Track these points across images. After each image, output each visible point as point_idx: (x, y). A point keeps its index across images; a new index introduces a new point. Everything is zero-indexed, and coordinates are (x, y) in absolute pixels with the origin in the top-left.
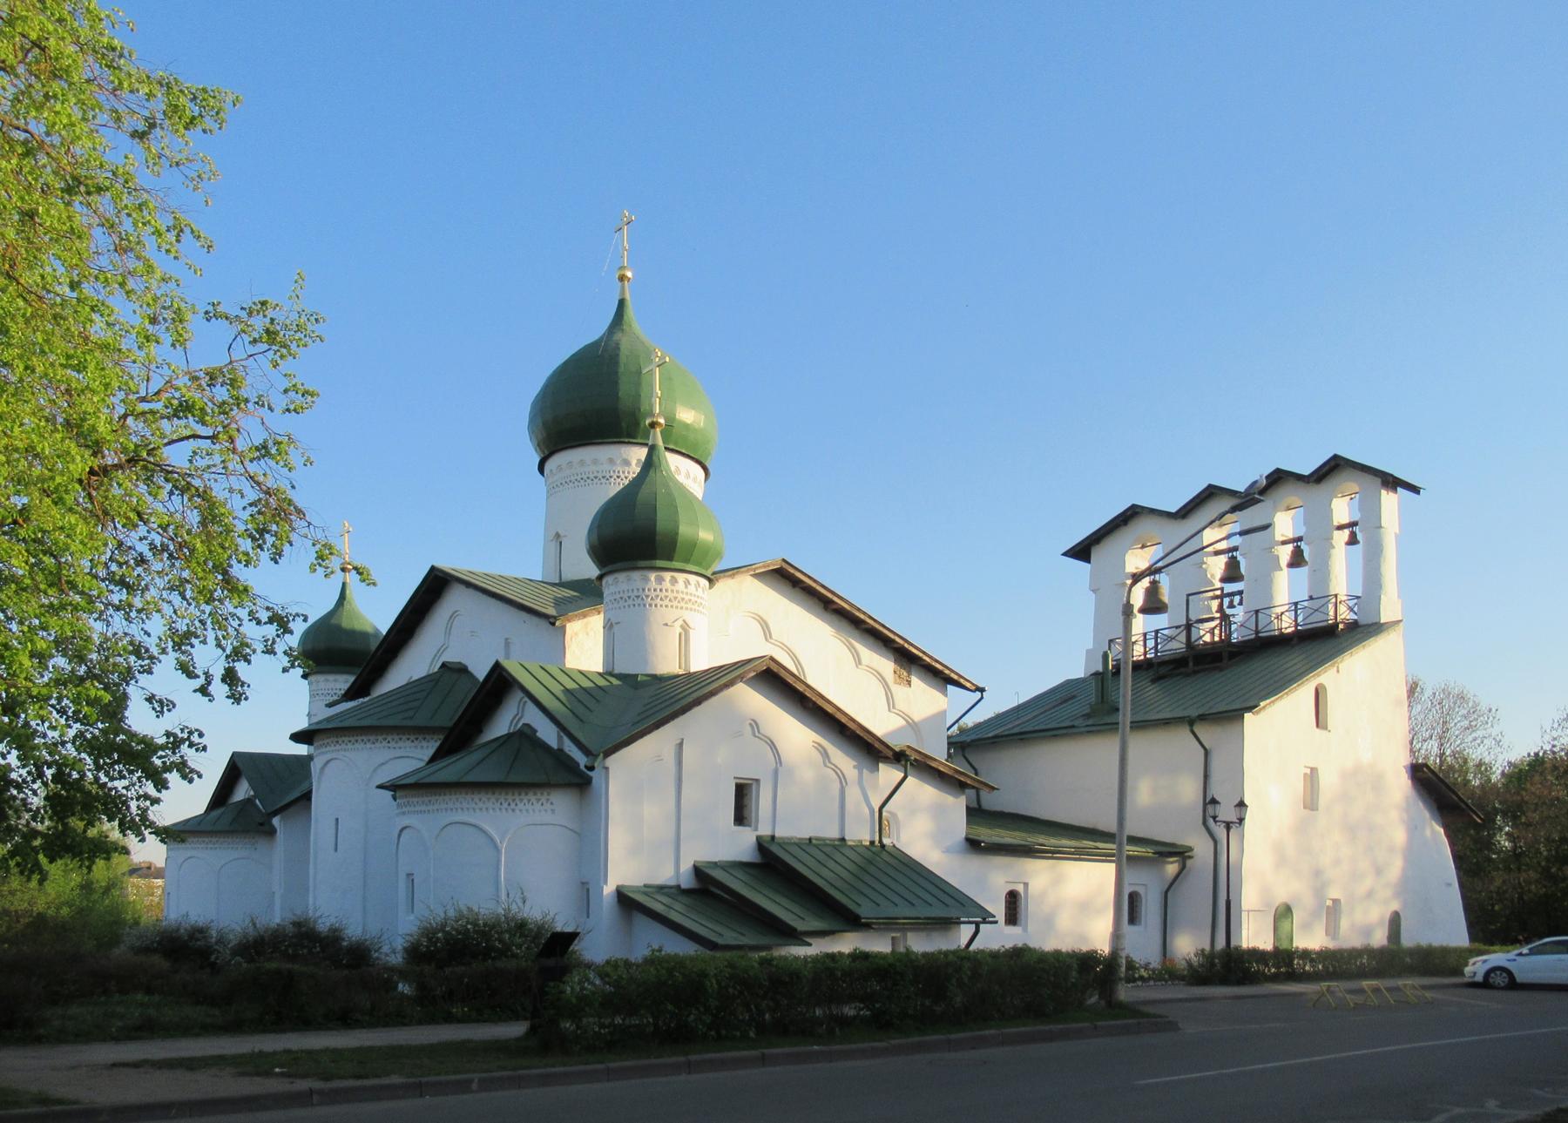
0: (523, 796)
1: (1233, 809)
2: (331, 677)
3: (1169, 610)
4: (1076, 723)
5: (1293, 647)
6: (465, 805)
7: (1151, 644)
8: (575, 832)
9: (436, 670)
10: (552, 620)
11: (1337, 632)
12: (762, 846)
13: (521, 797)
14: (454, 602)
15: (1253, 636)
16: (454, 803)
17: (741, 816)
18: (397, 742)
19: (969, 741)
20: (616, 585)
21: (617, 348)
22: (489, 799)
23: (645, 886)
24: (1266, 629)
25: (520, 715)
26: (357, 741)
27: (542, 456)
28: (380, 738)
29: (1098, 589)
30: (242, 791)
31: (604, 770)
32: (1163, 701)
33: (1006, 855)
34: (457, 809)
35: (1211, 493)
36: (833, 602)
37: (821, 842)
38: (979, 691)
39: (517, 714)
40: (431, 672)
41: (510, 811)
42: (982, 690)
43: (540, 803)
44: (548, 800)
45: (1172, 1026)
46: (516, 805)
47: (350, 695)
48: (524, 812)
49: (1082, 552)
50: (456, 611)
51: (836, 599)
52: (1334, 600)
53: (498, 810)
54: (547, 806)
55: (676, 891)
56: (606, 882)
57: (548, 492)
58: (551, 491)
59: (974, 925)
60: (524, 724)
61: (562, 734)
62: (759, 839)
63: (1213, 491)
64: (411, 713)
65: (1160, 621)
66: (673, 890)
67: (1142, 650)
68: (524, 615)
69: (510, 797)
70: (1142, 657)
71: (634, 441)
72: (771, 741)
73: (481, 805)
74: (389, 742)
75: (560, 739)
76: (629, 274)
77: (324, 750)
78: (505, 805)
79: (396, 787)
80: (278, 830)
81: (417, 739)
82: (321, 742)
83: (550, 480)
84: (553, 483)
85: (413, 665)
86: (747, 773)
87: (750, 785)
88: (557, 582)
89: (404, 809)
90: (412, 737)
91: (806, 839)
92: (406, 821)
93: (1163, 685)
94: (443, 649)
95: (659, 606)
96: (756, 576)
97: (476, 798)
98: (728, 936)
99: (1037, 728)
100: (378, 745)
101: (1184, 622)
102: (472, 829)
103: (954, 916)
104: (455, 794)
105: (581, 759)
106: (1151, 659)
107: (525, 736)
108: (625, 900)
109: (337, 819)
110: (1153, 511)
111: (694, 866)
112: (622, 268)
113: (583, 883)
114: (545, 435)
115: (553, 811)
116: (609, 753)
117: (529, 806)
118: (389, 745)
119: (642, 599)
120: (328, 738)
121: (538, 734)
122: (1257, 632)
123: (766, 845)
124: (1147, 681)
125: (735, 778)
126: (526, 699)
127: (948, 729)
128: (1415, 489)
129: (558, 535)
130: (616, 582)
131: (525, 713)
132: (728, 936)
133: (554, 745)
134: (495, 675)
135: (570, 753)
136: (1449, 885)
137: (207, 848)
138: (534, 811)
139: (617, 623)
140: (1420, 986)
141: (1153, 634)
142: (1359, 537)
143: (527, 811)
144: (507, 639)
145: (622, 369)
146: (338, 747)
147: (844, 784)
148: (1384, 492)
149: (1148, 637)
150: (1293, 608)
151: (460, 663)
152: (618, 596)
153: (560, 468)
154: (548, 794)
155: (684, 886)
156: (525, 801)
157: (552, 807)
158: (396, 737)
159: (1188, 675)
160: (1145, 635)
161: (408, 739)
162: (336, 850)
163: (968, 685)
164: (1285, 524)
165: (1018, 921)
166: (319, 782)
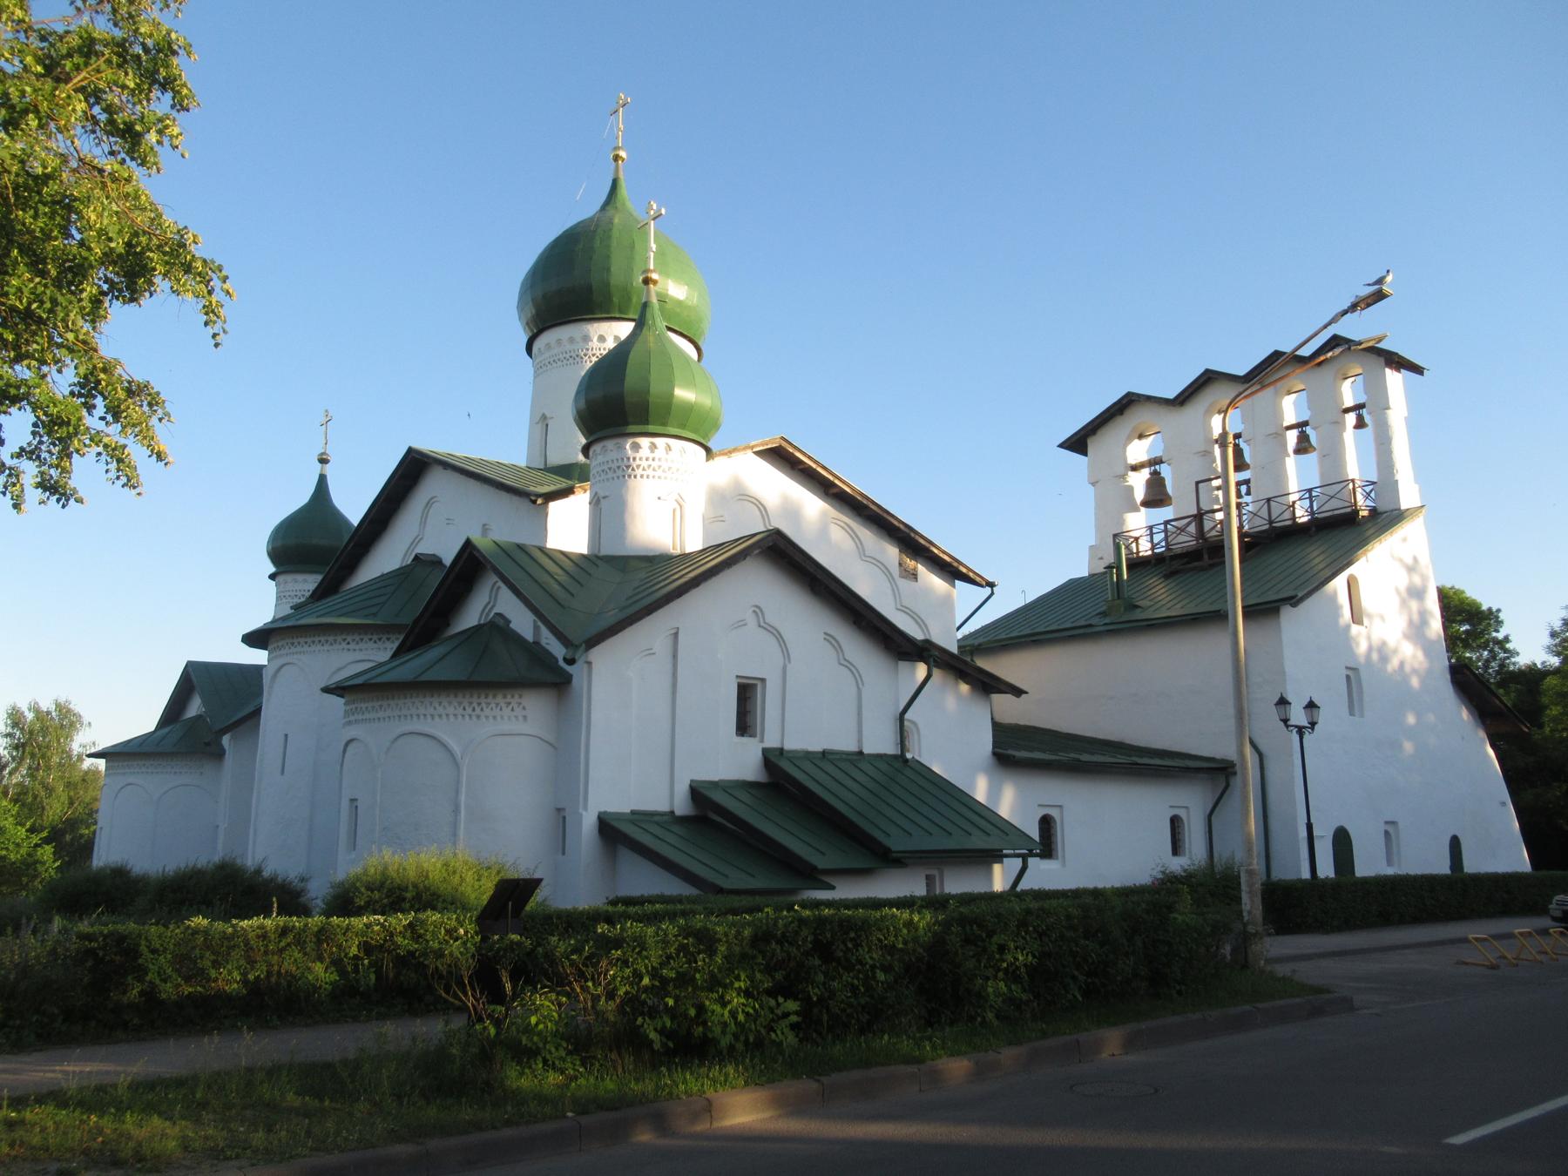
0: (490, 699)
1: (1303, 710)
2: (300, 577)
3: (1173, 501)
4: (1093, 622)
5: (1311, 536)
6: (422, 711)
7: (1158, 538)
8: (551, 744)
9: (409, 562)
10: (533, 498)
11: (1357, 520)
12: (771, 759)
13: (489, 701)
14: (433, 486)
15: (1267, 527)
16: (409, 709)
17: (745, 724)
18: (357, 643)
19: (976, 644)
20: (605, 452)
21: (611, 222)
22: (450, 703)
23: (633, 812)
24: (1277, 520)
25: (492, 604)
26: (313, 642)
27: (530, 334)
28: (339, 638)
29: (1097, 482)
30: (195, 708)
31: (586, 666)
32: (1169, 598)
33: (1158, 750)
34: (411, 716)
35: (1209, 378)
36: (835, 485)
37: (838, 757)
38: (989, 586)
39: (489, 603)
40: (404, 565)
41: (474, 718)
42: (991, 585)
43: (510, 707)
44: (520, 704)
45: (1347, 1005)
46: (482, 710)
47: (320, 594)
48: (491, 719)
49: (1078, 443)
50: (435, 497)
51: (837, 482)
52: (1351, 486)
53: (460, 717)
54: (518, 711)
55: (670, 819)
56: (586, 808)
57: (535, 372)
58: (539, 370)
59: (1020, 859)
60: (496, 614)
61: (539, 623)
62: (765, 751)
63: (1211, 376)
64: (374, 610)
65: (1166, 513)
66: (665, 818)
67: (1149, 545)
68: (504, 495)
69: (475, 700)
70: (1150, 553)
71: (626, 316)
72: (778, 632)
73: (440, 710)
74: (348, 643)
75: (536, 628)
76: (623, 154)
77: (278, 653)
78: (469, 710)
79: (338, 690)
80: (227, 752)
81: (380, 639)
82: (275, 645)
83: (537, 361)
84: (541, 362)
85: (387, 558)
86: (751, 671)
87: (755, 685)
88: (542, 467)
89: (352, 718)
90: (375, 637)
91: (820, 752)
92: (352, 732)
93: (1177, 581)
94: (417, 541)
95: (651, 477)
96: (758, 453)
97: (435, 701)
98: (734, 878)
99: (1048, 629)
100: (336, 646)
101: (1195, 512)
102: (422, 740)
103: (997, 847)
104: (411, 697)
105: (558, 650)
106: (1162, 553)
107: (497, 628)
108: (611, 831)
109: (286, 735)
110: (1149, 399)
111: (691, 787)
112: (617, 148)
113: (559, 810)
114: (534, 311)
115: (525, 717)
116: (594, 641)
117: (497, 712)
118: (349, 646)
119: (633, 470)
120: (283, 639)
121: (511, 625)
122: (1271, 522)
123: (773, 759)
124: (1159, 577)
125: (737, 677)
126: (500, 584)
127: (958, 628)
128: (1417, 369)
129: (544, 417)
130: (604, 449)
131: (499, 601)
132: (734, 878)
133: (529, 636)
134: (466, 555)
135: (547, 647)
136: (1504, 804)
137: (147, 773)
138: (502, 717)
139: (604, 498)
140: (1536, 931)
141: (1162, 527)
142: (1367, 419)
143: (495, 717)
144: (484, 525)
145: (614, 243)
146: (293, 649)
147: (861, 686)
148: (1388, 371)
149: (1155, 530)
150: (1307, 495)
151: (434, 555)
152: (605, 467)
153: (548, 346)
154: (520, 697)
155: (678, 812)
156: (494, 705)
157: (524, 713)
158: (357, 638)
159: (1203, 569)
160: (1151, 528)
161: (371, 639)
162: (283, 772)
163: (978, 579)
164: (1291, 408)
165: (1054, 853)
166: (271, 687)
